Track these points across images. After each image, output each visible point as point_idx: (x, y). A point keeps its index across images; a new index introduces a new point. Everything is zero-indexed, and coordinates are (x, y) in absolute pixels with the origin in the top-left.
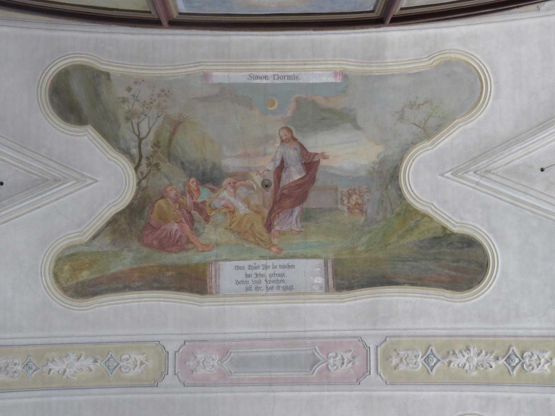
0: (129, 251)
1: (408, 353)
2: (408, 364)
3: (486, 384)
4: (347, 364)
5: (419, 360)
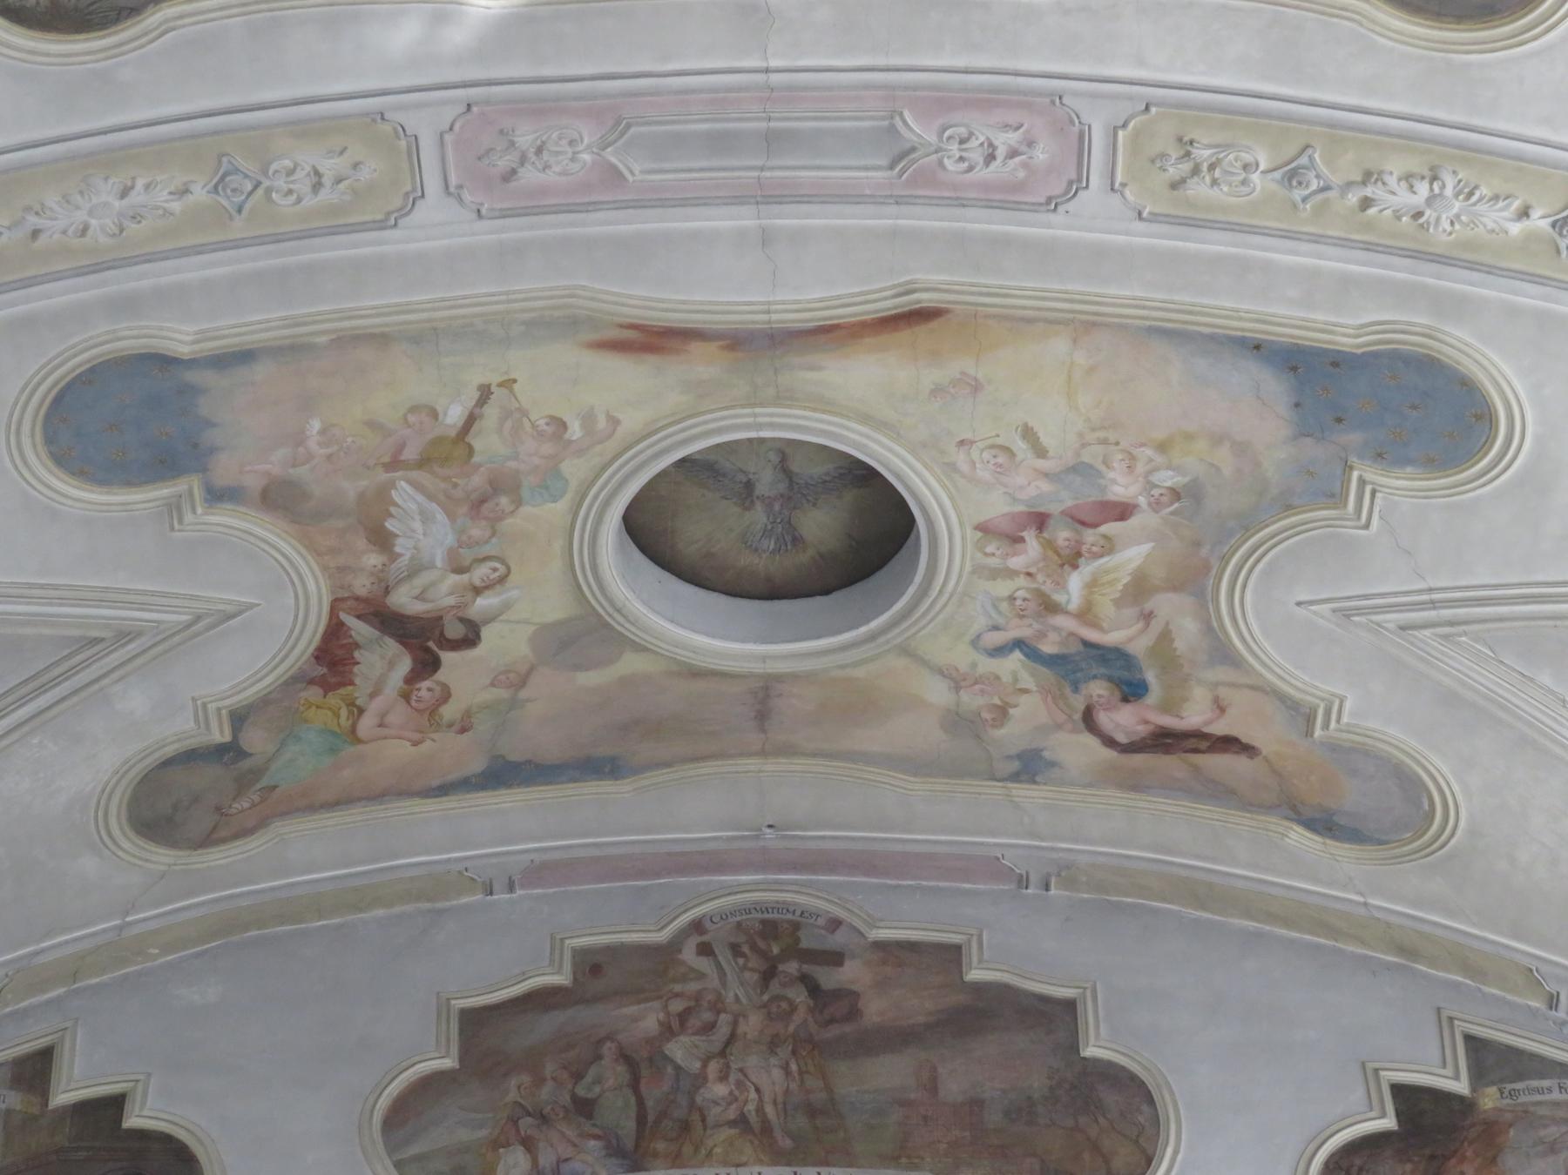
0: (976, 1104)
1: (1222, 155)
2: (1215, 182)
3: (1361, 245)
4: (1006, 158)
5: (1255, 177)
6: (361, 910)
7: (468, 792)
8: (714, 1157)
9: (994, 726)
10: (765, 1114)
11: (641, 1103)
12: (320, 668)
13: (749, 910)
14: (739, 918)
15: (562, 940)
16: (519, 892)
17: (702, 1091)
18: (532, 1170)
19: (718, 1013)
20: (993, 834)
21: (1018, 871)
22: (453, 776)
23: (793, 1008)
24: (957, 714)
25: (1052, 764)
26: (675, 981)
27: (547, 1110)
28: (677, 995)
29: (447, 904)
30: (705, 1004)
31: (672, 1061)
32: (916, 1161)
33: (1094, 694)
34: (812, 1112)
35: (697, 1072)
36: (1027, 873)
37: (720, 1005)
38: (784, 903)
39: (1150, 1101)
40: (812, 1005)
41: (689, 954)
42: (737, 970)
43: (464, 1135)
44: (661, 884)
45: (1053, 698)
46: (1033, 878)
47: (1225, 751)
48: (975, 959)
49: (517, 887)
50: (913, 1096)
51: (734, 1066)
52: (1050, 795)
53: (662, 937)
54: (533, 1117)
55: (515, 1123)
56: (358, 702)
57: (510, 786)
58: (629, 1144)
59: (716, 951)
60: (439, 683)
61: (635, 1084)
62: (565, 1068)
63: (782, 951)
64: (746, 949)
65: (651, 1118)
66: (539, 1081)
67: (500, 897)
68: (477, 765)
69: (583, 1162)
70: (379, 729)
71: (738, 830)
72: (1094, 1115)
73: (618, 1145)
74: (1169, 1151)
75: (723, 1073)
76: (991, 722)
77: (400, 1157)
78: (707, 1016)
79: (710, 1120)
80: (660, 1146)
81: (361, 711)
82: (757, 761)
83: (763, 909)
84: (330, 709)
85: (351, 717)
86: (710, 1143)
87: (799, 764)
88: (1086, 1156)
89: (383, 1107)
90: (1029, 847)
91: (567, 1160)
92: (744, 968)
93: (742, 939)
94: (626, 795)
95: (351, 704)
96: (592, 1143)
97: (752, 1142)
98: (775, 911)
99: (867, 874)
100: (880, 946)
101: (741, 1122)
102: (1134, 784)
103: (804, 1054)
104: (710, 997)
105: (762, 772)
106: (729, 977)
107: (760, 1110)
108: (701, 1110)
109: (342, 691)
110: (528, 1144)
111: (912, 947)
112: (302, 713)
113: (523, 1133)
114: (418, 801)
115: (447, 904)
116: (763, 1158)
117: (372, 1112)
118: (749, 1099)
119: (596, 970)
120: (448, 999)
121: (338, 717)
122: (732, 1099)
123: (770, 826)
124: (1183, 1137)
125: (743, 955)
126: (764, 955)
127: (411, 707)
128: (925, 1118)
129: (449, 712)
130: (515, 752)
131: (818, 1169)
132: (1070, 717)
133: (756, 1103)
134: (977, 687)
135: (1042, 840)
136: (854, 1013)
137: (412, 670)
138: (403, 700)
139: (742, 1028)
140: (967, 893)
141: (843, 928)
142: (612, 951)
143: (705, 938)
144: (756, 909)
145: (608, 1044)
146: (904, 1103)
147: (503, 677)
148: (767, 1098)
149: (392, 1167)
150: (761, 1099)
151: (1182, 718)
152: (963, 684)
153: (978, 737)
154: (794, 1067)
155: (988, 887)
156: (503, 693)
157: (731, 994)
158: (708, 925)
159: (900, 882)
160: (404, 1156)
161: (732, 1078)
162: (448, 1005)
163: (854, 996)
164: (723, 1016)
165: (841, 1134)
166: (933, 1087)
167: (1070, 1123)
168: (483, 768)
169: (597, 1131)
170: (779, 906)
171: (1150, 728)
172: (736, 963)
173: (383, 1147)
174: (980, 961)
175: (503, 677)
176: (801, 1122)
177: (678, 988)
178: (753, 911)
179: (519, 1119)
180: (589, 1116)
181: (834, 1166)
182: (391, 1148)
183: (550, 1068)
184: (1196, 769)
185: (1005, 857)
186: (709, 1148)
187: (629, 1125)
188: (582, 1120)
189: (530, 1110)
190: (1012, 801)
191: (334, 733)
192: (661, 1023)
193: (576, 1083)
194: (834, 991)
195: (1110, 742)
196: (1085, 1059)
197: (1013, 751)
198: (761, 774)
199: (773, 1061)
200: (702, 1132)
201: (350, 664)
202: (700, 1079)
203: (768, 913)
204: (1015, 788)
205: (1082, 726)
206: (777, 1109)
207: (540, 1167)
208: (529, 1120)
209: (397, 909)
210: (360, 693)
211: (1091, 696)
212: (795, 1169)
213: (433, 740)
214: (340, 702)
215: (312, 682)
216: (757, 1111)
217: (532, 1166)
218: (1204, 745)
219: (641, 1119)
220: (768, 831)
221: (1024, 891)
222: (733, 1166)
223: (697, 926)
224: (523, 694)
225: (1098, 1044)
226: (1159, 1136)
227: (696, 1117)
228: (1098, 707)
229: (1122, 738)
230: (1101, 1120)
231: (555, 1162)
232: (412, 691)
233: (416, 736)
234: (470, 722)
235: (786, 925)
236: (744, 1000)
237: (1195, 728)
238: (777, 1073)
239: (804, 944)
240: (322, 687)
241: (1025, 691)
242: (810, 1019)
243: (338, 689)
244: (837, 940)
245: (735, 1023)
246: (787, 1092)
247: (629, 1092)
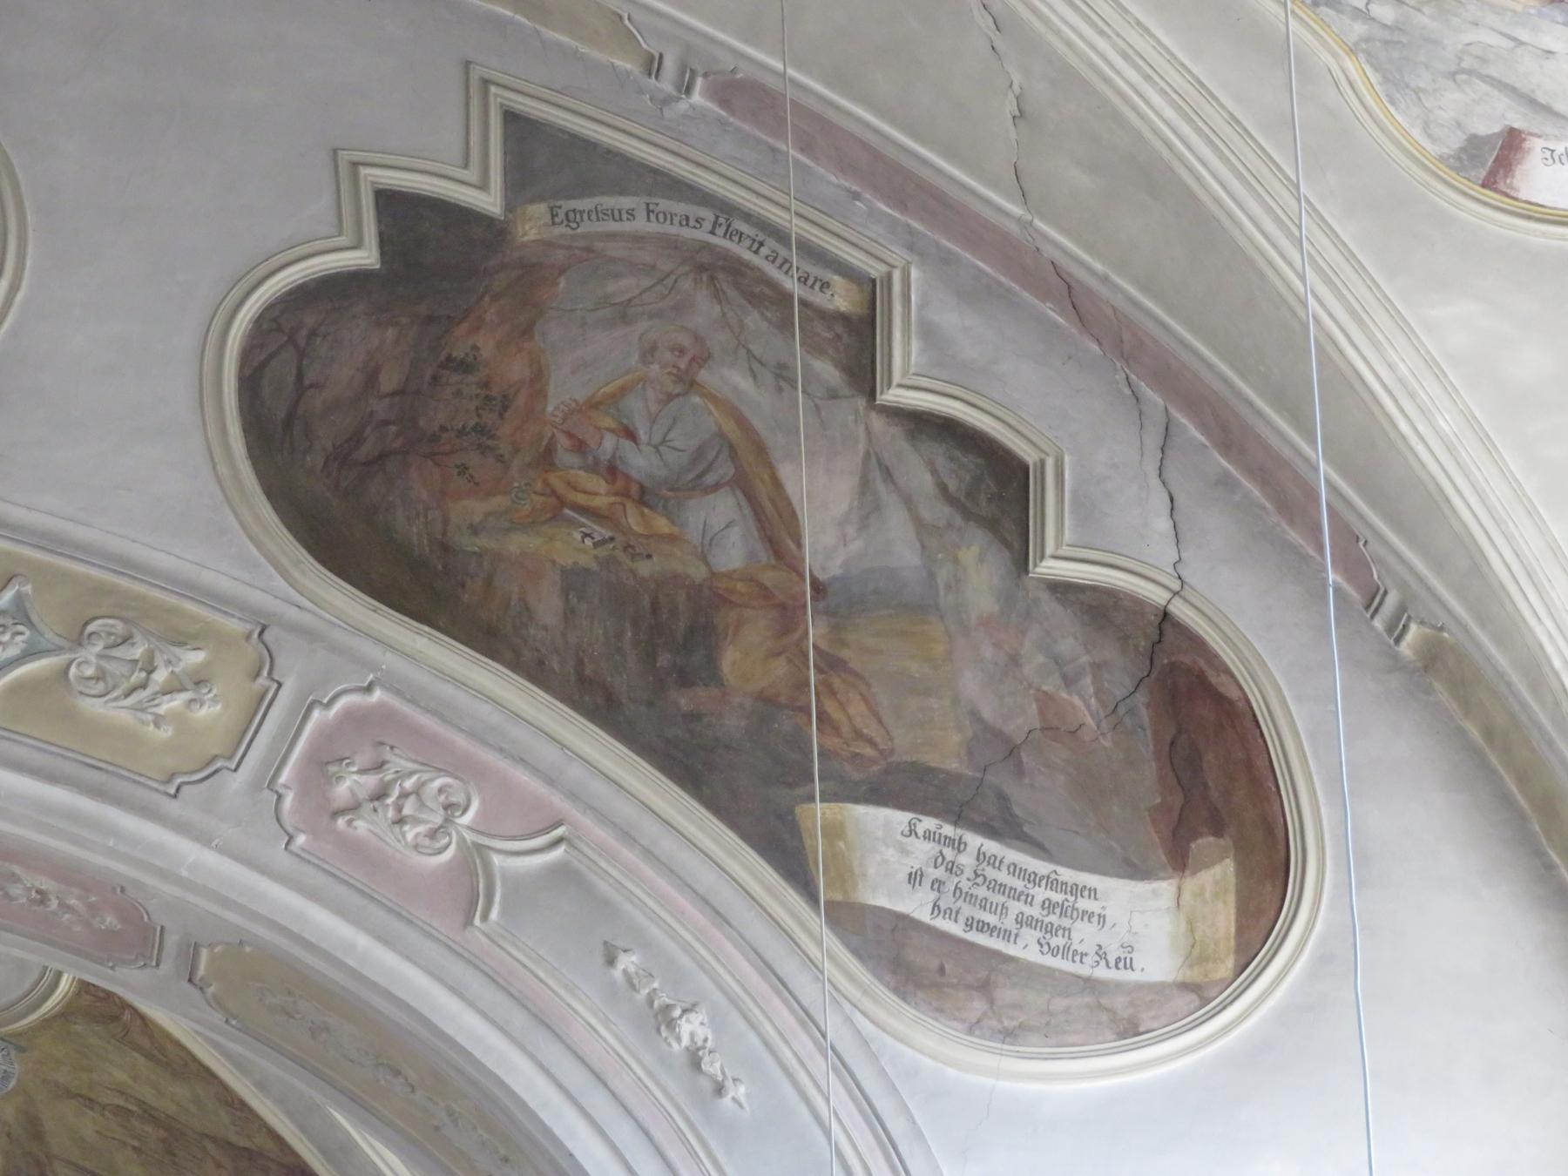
124: (29, 263)
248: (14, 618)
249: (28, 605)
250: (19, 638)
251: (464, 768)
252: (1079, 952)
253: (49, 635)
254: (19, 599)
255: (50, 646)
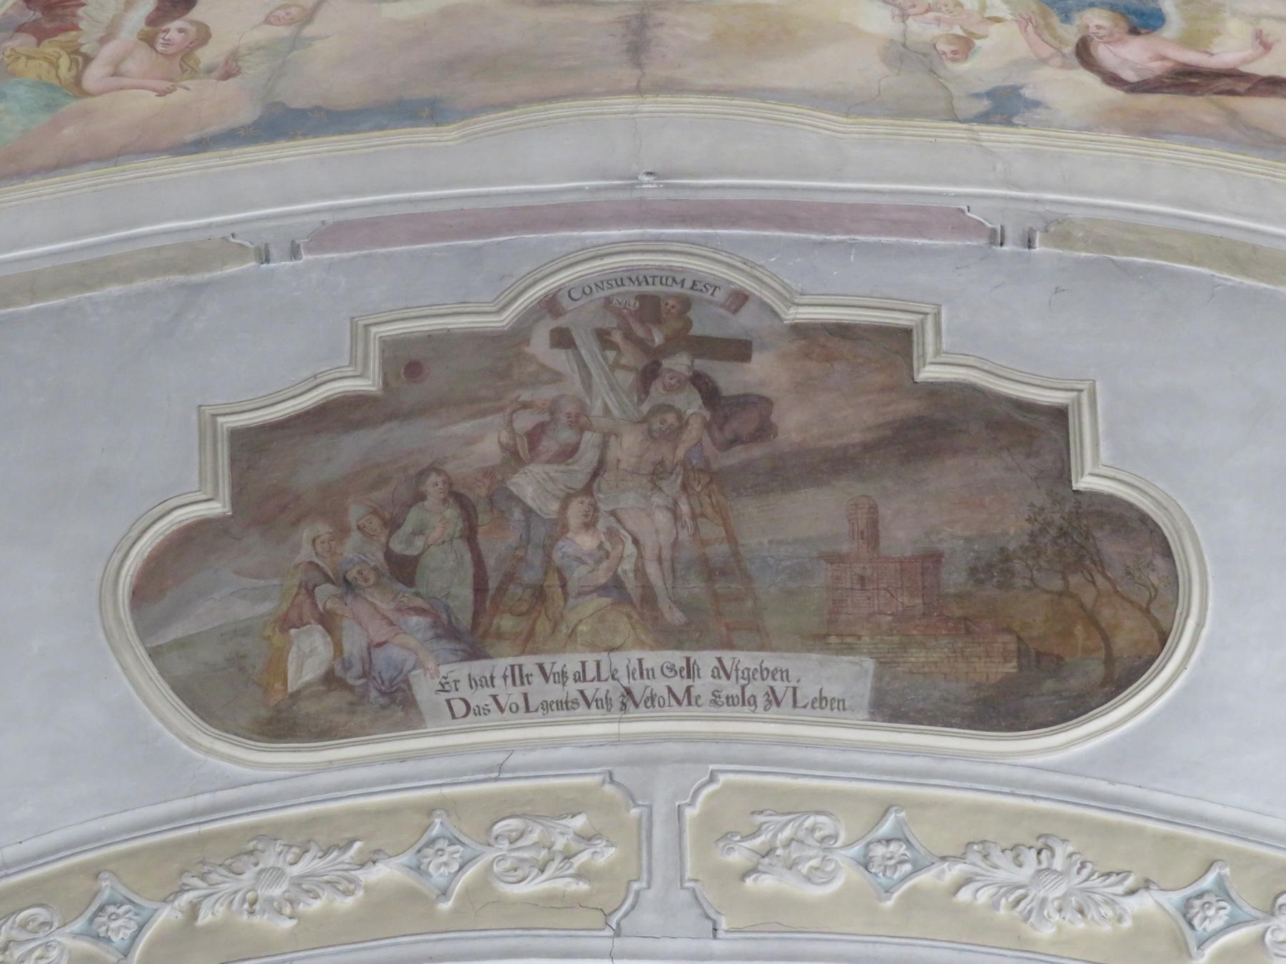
6: (89, 288)
7: (235, 146)
8: (579, 639)
9: (954, 60)
10: (645, 574)
11: (479, 562)
12: (32, 12)
13: (622, 280)
14: (607, 293)
15: (367, 326)
16: (306, 257)
17: (560, 543)
18: (334, 659)
19: (582, 430)
20: (955, 181)
21: (990, 226)
22: (214, 129)
23: (683, 423)
24: (904, 45)
25: (1037, 104)
26: (521, 385)
27: (352, 575)
28: (525, 406)
29: (207, 276)
30: (563, 419)
31: (519, 501)
32: (849, 640)
33: (1091, 25)
34: (710, 571)
35: (554, 516)
36: (1002, 227)
37: (583, 420)
38: (670, 269)
39: (1168, 553)
40: (708, 417)
41: (540, 345)
42: (607, 369)
43: (243, 611)
44: (499, 243)
45: (1036, 28)
46: (1009, 233)
47: (1273, 94)
48: (930, 349)
49: (303, 252)
50: (845, 548)
51: (603, 507)
52: (1033, 139)
53: (502, 321)
54: (333, 583)
55: (311, 593)
56: (83, 49)
57: (292, 137)
58: (465, 619)
59: (578, 342)
60: (192, 22)
61: (470, 535)
62: (375, 512)
63: (667, 339)
64: (617, 337)
65: (493, 584)
66: (342, 532)
67: (281, 265)
68: (247, 114)
69: (404, 647)
70: (112, 78)
71: (604, 178)
72: (1091, 575)
73: (450, 622)
74: (1191, 623)
75: (589, 518)
76: (950, 56)
77: (155, 644)
78: (567, 436)
79: (573, 587)
80: (506, 623)
81: (88, 59)
82: (630, 100)
83: (641, 278)
84: (45, 59)
85: (74, 67)
86: (572, 618)
87: (689, 103)
88: (1079, 631)
89: (131, 573)
90: (1004, 198)
91: (380, 645)
92: (616, 365)
93: (611, 322)
94: (450, 143)
95: (75, 51)
96: (414, 620)
97: (630, 617)
98: (657, 281)
99: (782, 227)
100: (799, 330)
101: (615, 586)
102: (1148, 128)
103: (698, 489)
104: (570, 408)
105: (636, 112)
106: (596, 378)
107: (640, 571)
108: (559, 571)
109: (62, 38)
110: (328, 622)
111: (843, 331)
112: (8, 65)
113: (320, 607)
114: (165, 159)
115: (207, 276)
116: (643, 637)
117: (116, 582)
118: (625, 556)
119: (414, 370)
120: (214, 416)
121: (57, 67)
122: (602, 554)
123: (649, 174)
124: (1211, 604)
125: (614, 346)
126: (642, 345)
127: (156, 51)
128: (862, 579)
129: (207, 55)
130: (296, 94)
131: (718, 654)
132: (1059, 50)
133: (633, 560)
134: (931, 15)
135: (1023, 189)
136: (764, 431)
137: (158, 9)
138: (143, 43)
139: (613, 453)
140: (922, 250)
141: (749, 308)
142: (441, 343)
143: (561, 322)
144: (630, 279)
145: (433, 478)
146: (834, 559)
147: (281, 13)
148: (649, 553)
149: (146, 657)
150: (640, 556)
151: (1212, 55)
152: (912, 11)
153: (932, 71)
154: (684, 508)
155: (948, 243)
156: (283, 31)
157: (599, 403)
158: (565, 302)
159: (828, 237)
160: (161, 642)
161: (601, 526)
162: (214, 424)
163: (765, 403)
164: (587, 436)
165: (750, 603)
166: (872, 534)
167: (1057, 584)
168: (256, 118)
169: (419, 602)
170: (662, 273)
171: (1168, 65)
172: (605, 358)
173: (133, 632)
174: (938, 352)
175: (281, 13)
176: (695, 586)
177: (525, 396)
178: (626, 282)
179: (315, 586)
180: (409, 581)
181: (741, 648)
182: (144, 631)
183: (355, 513)
184: (1233, 115)
185: (971, 209)
186: (572, 626)
187: (464, 594)
188: (400, 586)
189: (330, 573)
190: (981, 146)
191: (51, 87)
192: (504, 447)
193: (390, 535)
194: (738, 397)
195: (1113, 80)
196: (1077, 492)
197: (982, 88)
198: (636, 115)
199: (657, 500)
200: (562, 603)
201: (73, 6)
202: (559, 528)
203: (647, 284)
204: (983, 131)
205: (1075, 61)
206: (662, 570)
207: (346, 655)
208: (329, 588)
209: (140, 285)
210: (87, 37)
211: (1088, 27)
212: (688, 654)
213: (187, 89)
214: (58, 50)
215: (20, 29)
216: (636, 571)
217: (335, 651)
218: (1242, 87)
219: (480, 587)
220: (646, 179)
221: (999, 248)
222: (605, 651)
223: (550, 305)
224: (309, 31)
225: (1097, 471)
226: (1177, 604)
227: (553, 580)
228: (1096, 39)
229: (1130, 75)
230: (1100, 580)
231: (365, 650)
232: (157, 33)
233: (165, 85)
234: (237, 66)
235: (671, 302)
236: (616, 412)
237: (1232, 67)
238: (662, 518)
239: (696, 330)
240: (34, 35)
241: (998, 20)
242: (706, 440)
243: (56, 36)
244: (743, 323)
245: (604, 446)
246: (675, 544)
247: (462, 547)
248: (1216, 896)
249: (1227, 884)
250: (1222, 912)
251: (820, 803)
252: (836, 699)
253: (1247, 909)
254: (1220, 881)
255: (1248, 918)
